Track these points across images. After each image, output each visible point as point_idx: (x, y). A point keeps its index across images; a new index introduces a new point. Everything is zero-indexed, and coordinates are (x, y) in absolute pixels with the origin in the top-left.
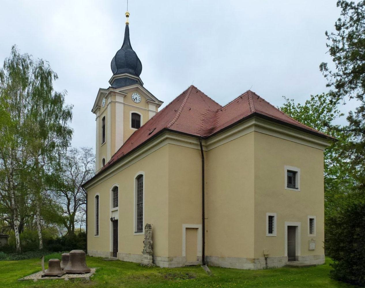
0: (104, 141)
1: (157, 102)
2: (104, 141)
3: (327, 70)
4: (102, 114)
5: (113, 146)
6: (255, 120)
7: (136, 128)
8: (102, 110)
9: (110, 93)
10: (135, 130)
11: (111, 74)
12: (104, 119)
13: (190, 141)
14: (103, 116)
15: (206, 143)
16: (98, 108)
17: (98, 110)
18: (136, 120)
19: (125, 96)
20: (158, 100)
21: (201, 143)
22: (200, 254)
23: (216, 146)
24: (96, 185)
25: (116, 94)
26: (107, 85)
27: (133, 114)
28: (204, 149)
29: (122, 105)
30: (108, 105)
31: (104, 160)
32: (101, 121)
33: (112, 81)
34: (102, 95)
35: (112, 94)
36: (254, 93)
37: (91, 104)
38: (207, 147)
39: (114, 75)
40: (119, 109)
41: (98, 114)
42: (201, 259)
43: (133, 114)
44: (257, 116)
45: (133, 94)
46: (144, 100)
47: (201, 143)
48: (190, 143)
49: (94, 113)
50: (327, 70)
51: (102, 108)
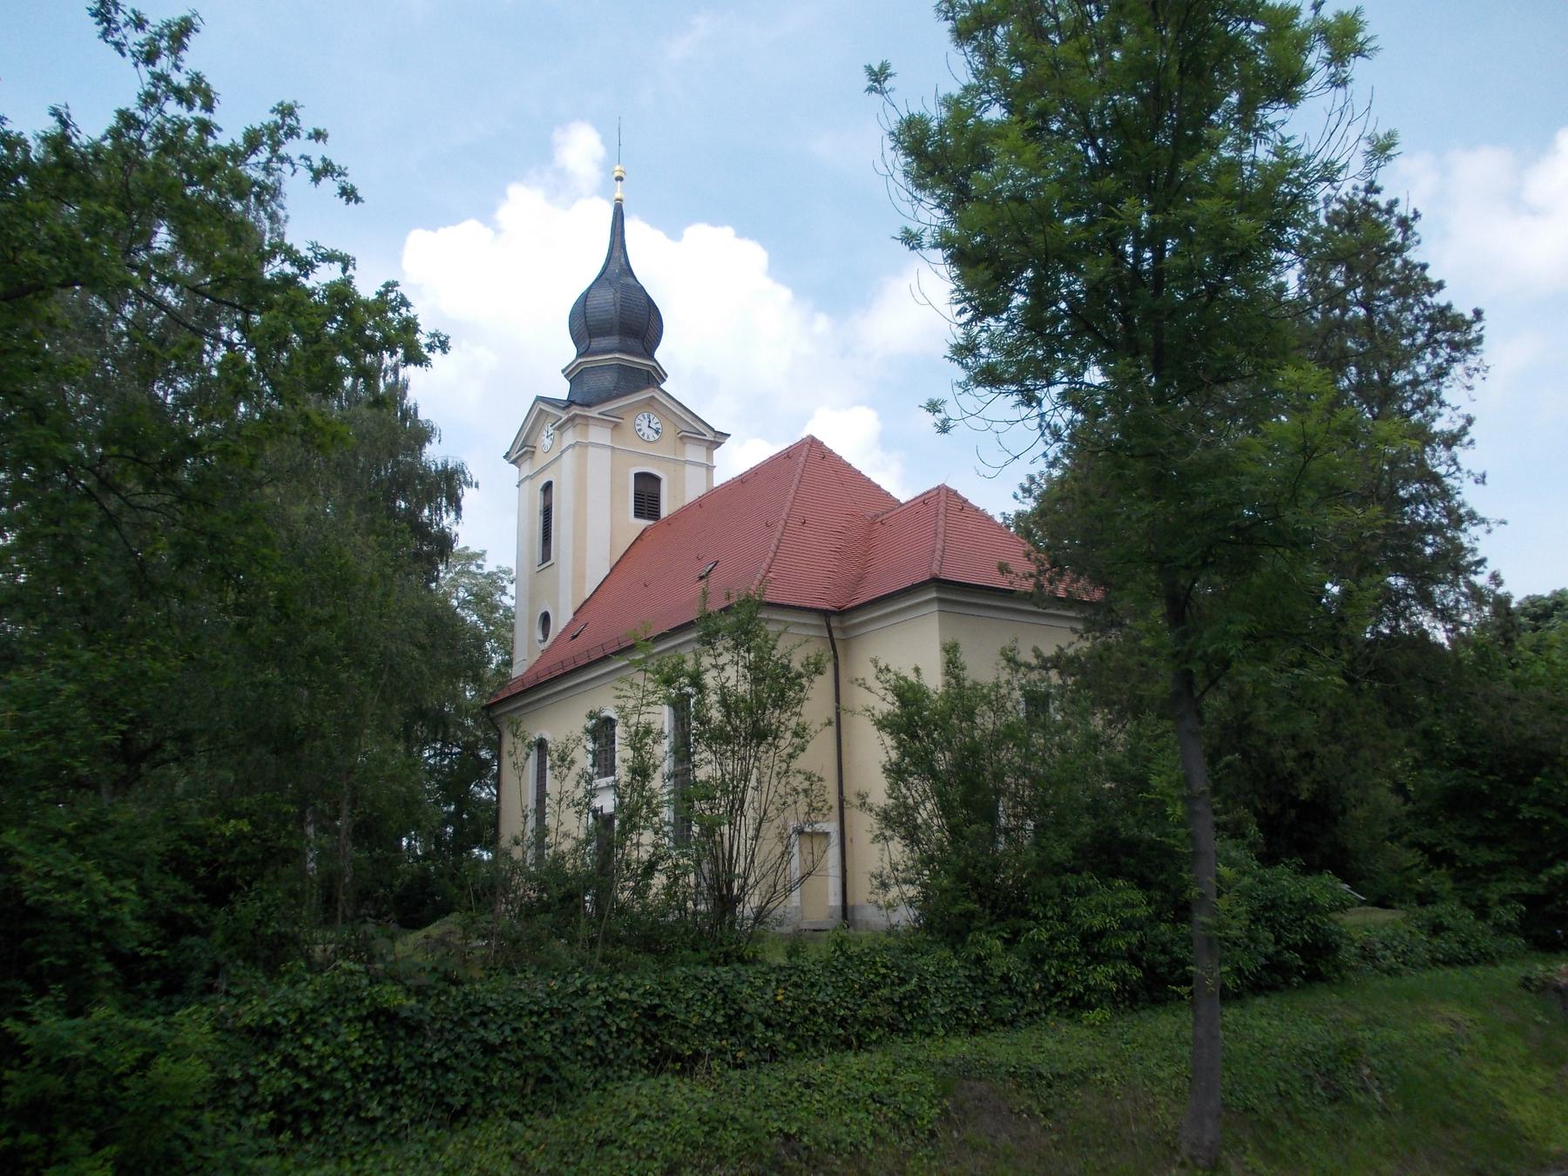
0: (546, 556)
1: (710, 437)
2: (546, 556)
3: (1010, 572)
4: (543, 469)
5: (579, 577)
6: (938, 591)
7: (649, 519)
8: (541, 459)
9: (571, 419)
10: (644, 523)
11: (568, 352)
12: (548, 487)
13: (802, 621)
14: (543, 480)
15: (841, 622)
16: (526, 452)
17: (528, 455)
18: (647, 495)
19: (616, 426)
20: (713, 429)
21: (828, 625)
22: (834, 901)
23: (863, 630)
24: (537, 706)
25: (591, 421)
26: (561, 389)
27: (639, 476)
28: (836, 635)
29: (607, 453)
30: (562, 452)
31: (546, 618)
32: (539, 496)
33: (575, 375)
34: (543, 417)
35: (578, 421)
36: (955, 493)
37: (506, 438)
38: (844, 630)
39: (579, 356)
40: (599, 464)
41: (527, 469)
42: (839, 913)
43: (639, 476)
44: (937, 582)
45: (640, 417)
46: (669, 432)
47: (828, 625)
48: (805, 624)
49: (514, 462)
50: (1010, 572)
51: (539, 453)
